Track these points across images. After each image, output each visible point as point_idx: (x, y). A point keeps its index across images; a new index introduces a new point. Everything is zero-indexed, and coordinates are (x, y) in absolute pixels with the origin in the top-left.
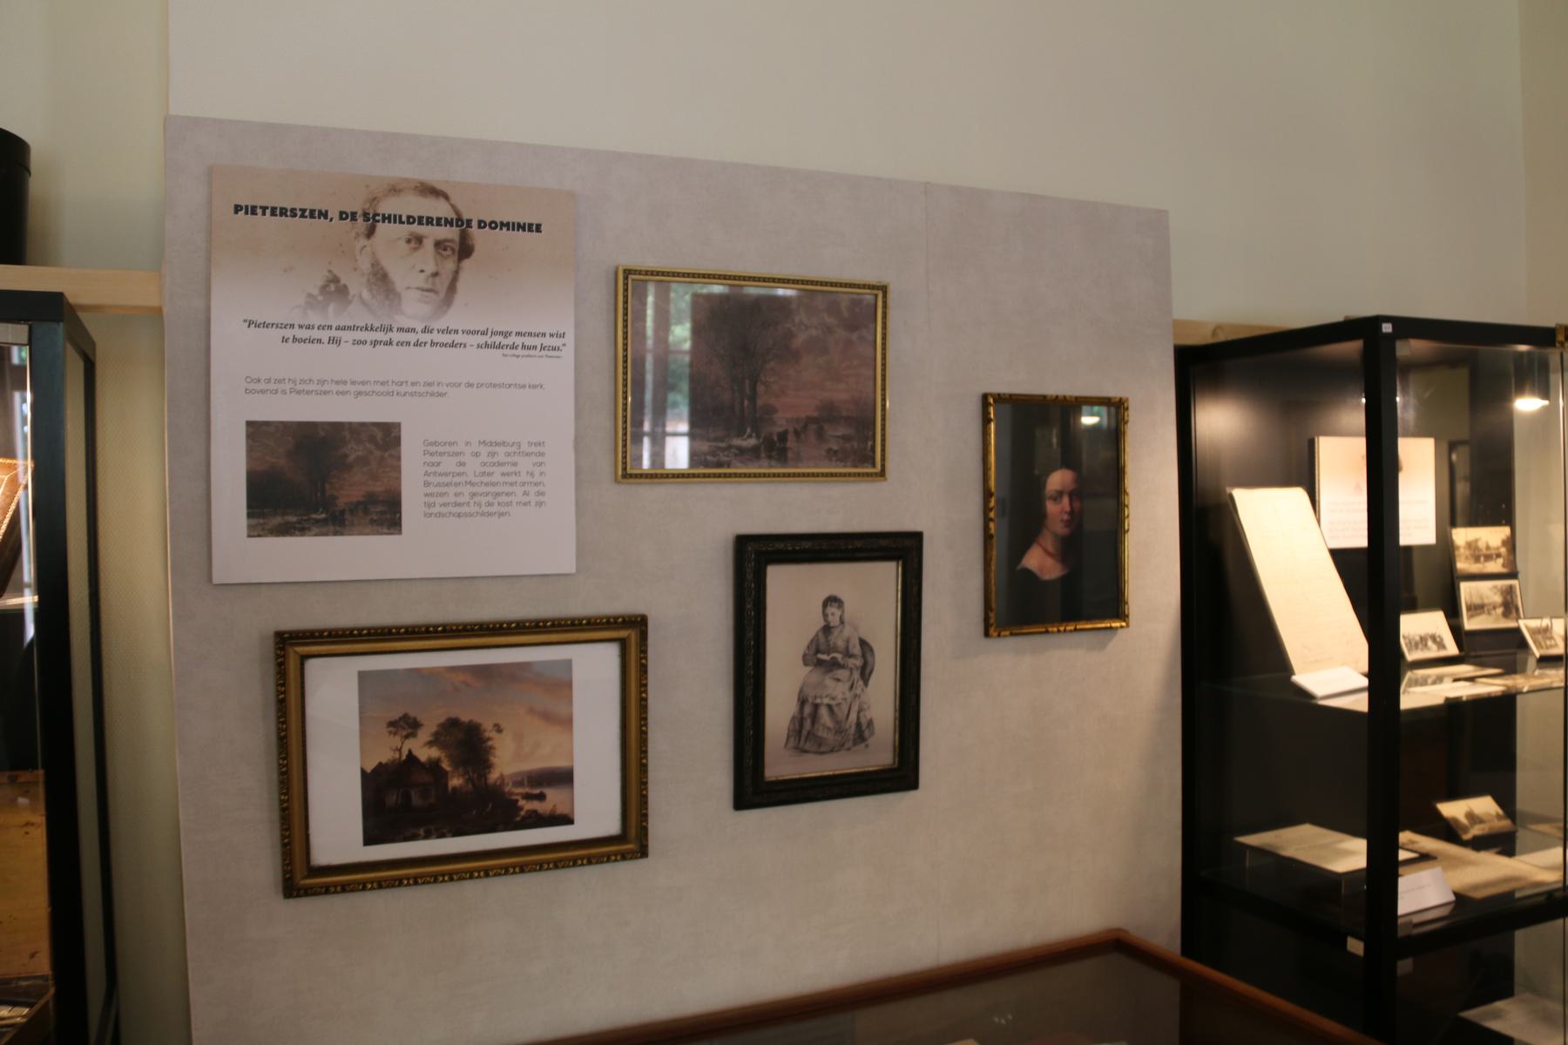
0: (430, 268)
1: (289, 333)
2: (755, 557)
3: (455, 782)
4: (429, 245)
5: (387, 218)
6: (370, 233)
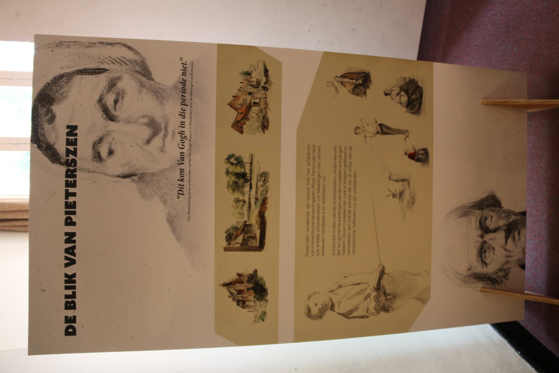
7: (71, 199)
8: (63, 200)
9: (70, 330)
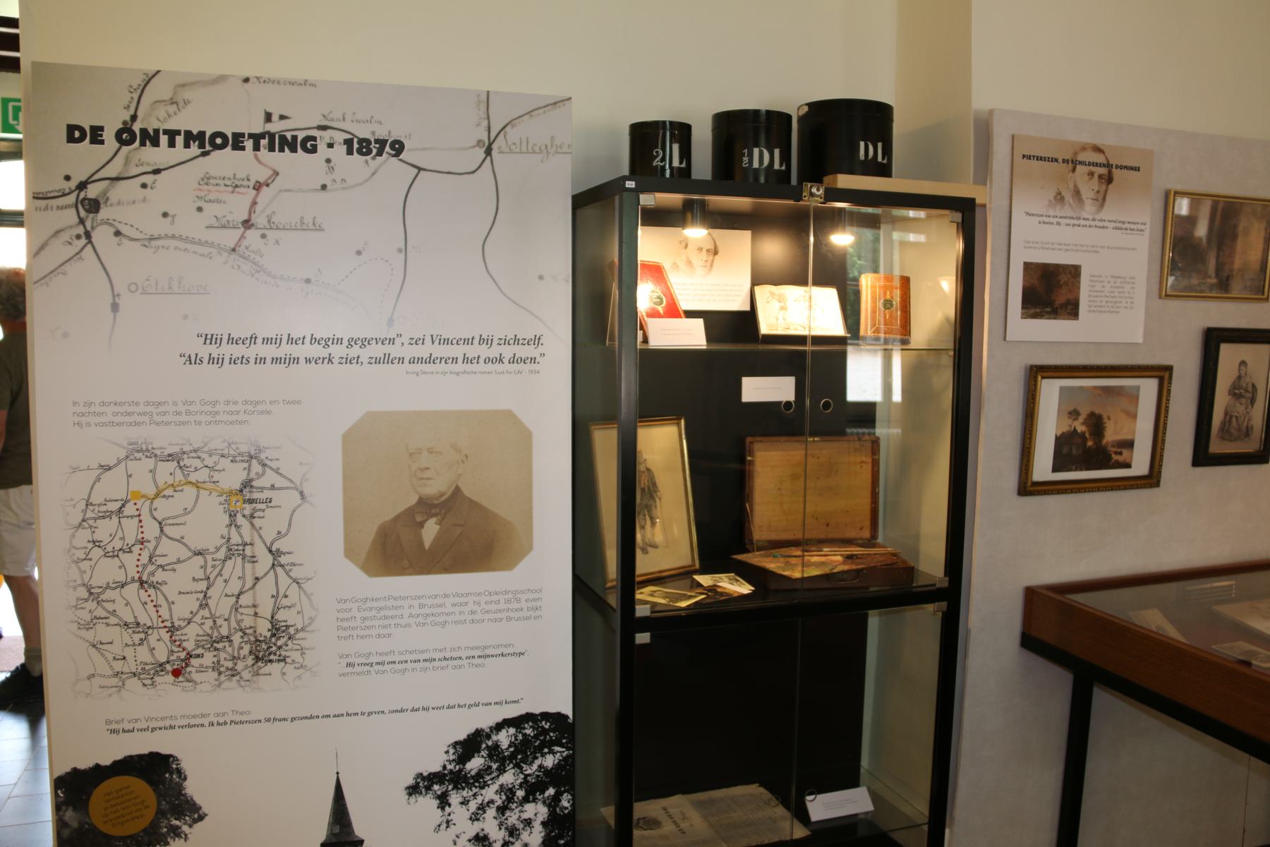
0: (1096, 188)
1: (1041, 219)
2: (1213, 339)
3: (1090, 443)
4: (1096, 176)
5: (1081, 163)
6: (1074, 170)
7: (164, 139)
8: (246, 131)
9: (77, 134)
